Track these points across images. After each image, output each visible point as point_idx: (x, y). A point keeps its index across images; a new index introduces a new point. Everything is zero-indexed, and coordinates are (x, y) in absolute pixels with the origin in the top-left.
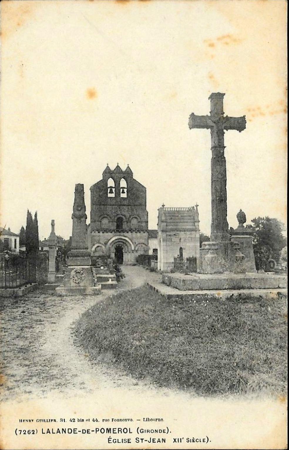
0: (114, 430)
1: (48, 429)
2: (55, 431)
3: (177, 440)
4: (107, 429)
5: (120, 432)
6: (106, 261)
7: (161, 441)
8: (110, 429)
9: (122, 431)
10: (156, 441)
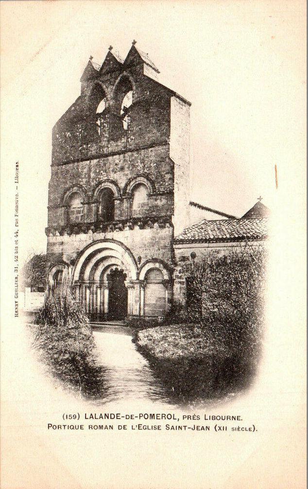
0: (158, 415)
1: (91, 414)
2: (98, 416)
3: (222, 428)
4: (151, 415)
5: (164, 418)
6: (139, 224)
7: (104, 417)
8: (154, 415)
9: (166, 417)
10: (200, 428)
